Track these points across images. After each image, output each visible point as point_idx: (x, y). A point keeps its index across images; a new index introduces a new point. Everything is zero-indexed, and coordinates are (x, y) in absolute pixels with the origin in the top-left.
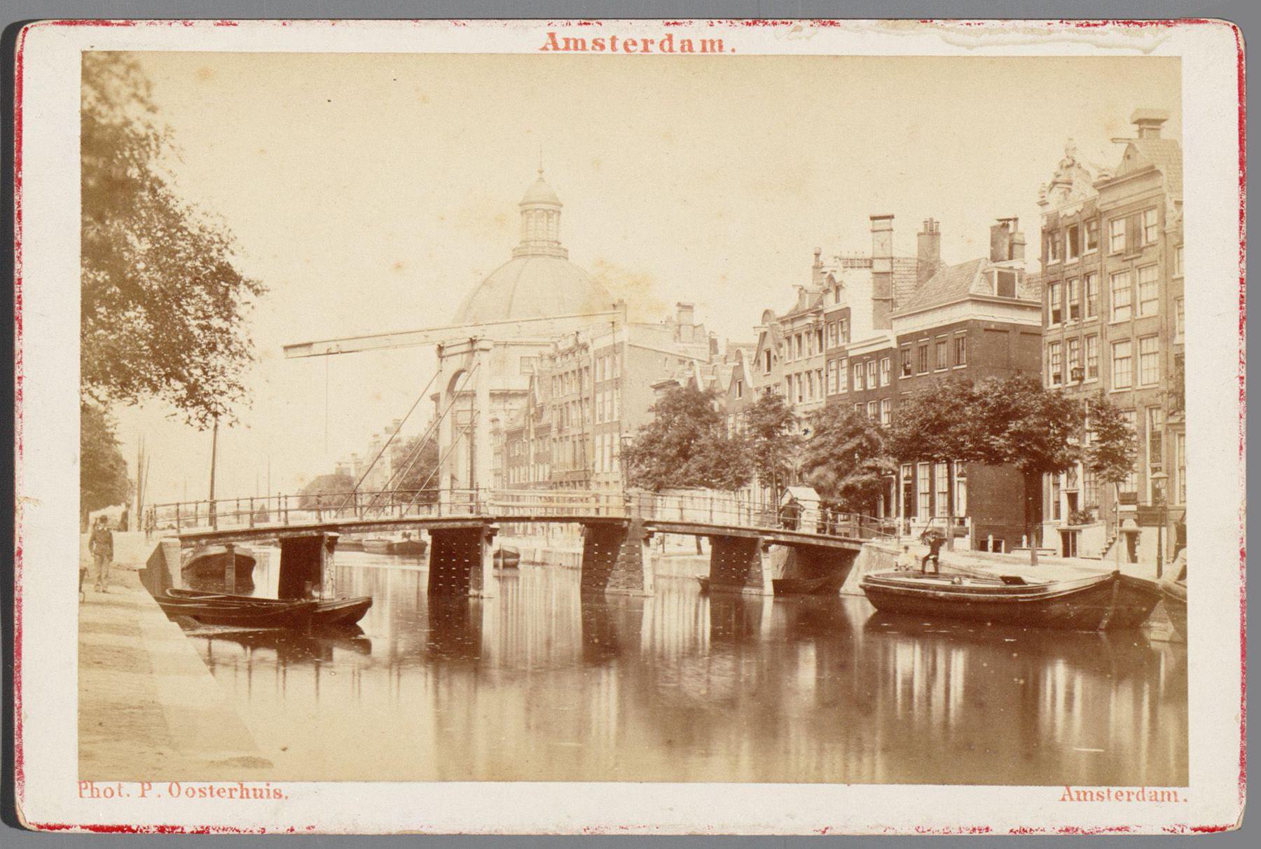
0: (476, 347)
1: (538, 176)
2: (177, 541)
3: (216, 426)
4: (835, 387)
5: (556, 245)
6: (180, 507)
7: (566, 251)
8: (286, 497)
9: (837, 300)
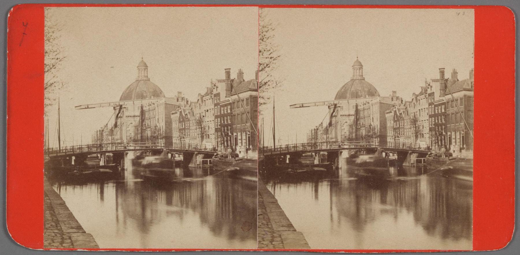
3: (263, 121)
4: (217, 113)
9: (431, 90)
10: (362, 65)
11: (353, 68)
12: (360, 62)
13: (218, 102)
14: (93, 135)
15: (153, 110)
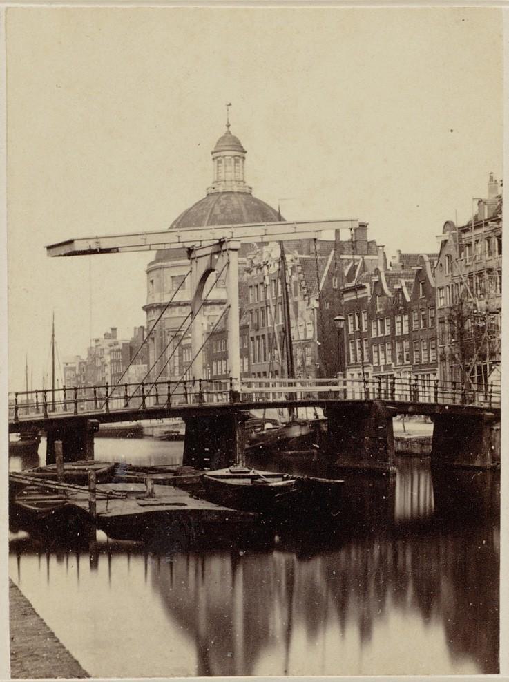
0: (224, 248)
1: (226, 129)
5: (242, 184)
6: (18, 396)
7: (251, 188)
8: (200, 381)
10: (242, 147)
11: (213, 159)
12: (235, 137)
14: (67, 364)
15: (257, 286)
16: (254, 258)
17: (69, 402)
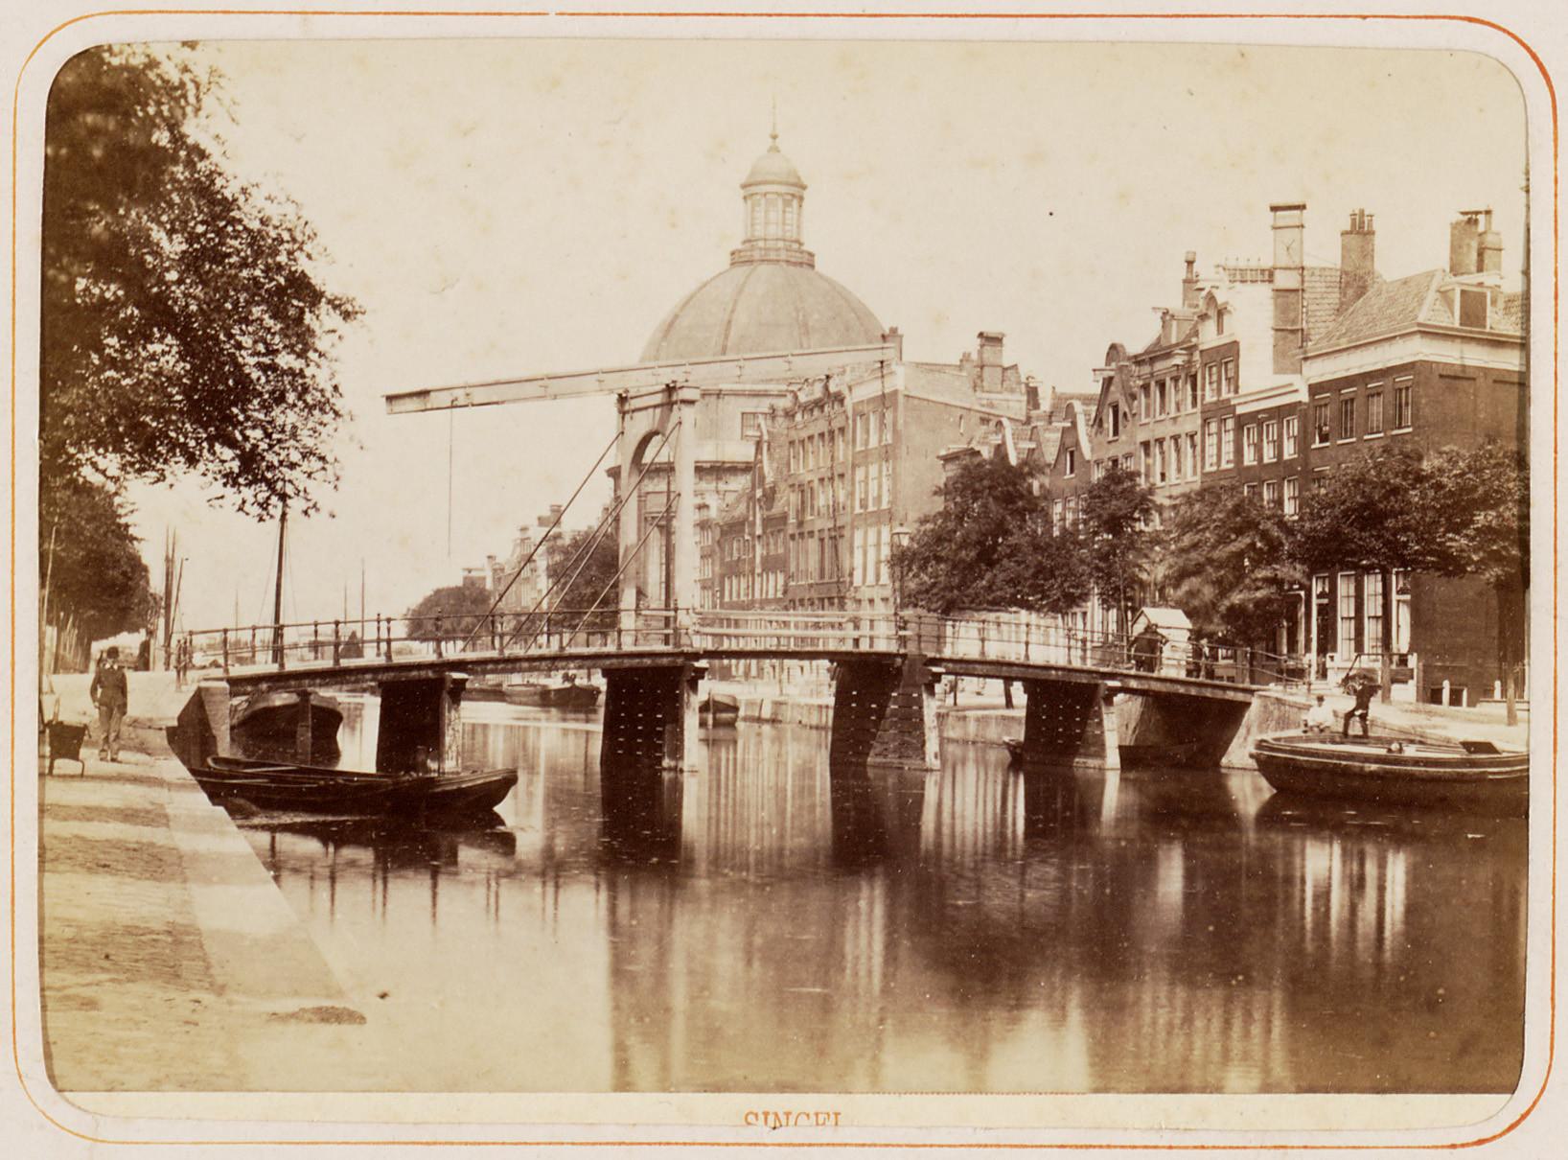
0: (674, 398)
2: (225, 684)
5: (795, 246)
7: (811, 255)
9: (1220, 330)
13: (1225, 395)
16: (800, 390)
17: (383, 640)
